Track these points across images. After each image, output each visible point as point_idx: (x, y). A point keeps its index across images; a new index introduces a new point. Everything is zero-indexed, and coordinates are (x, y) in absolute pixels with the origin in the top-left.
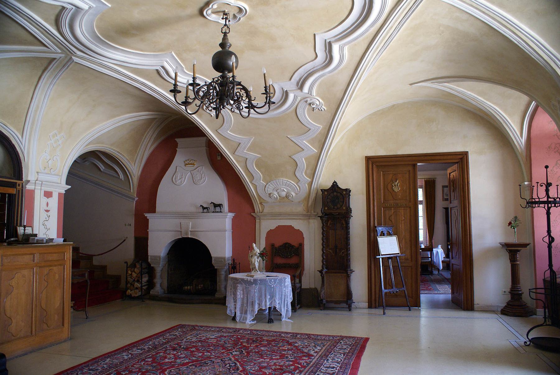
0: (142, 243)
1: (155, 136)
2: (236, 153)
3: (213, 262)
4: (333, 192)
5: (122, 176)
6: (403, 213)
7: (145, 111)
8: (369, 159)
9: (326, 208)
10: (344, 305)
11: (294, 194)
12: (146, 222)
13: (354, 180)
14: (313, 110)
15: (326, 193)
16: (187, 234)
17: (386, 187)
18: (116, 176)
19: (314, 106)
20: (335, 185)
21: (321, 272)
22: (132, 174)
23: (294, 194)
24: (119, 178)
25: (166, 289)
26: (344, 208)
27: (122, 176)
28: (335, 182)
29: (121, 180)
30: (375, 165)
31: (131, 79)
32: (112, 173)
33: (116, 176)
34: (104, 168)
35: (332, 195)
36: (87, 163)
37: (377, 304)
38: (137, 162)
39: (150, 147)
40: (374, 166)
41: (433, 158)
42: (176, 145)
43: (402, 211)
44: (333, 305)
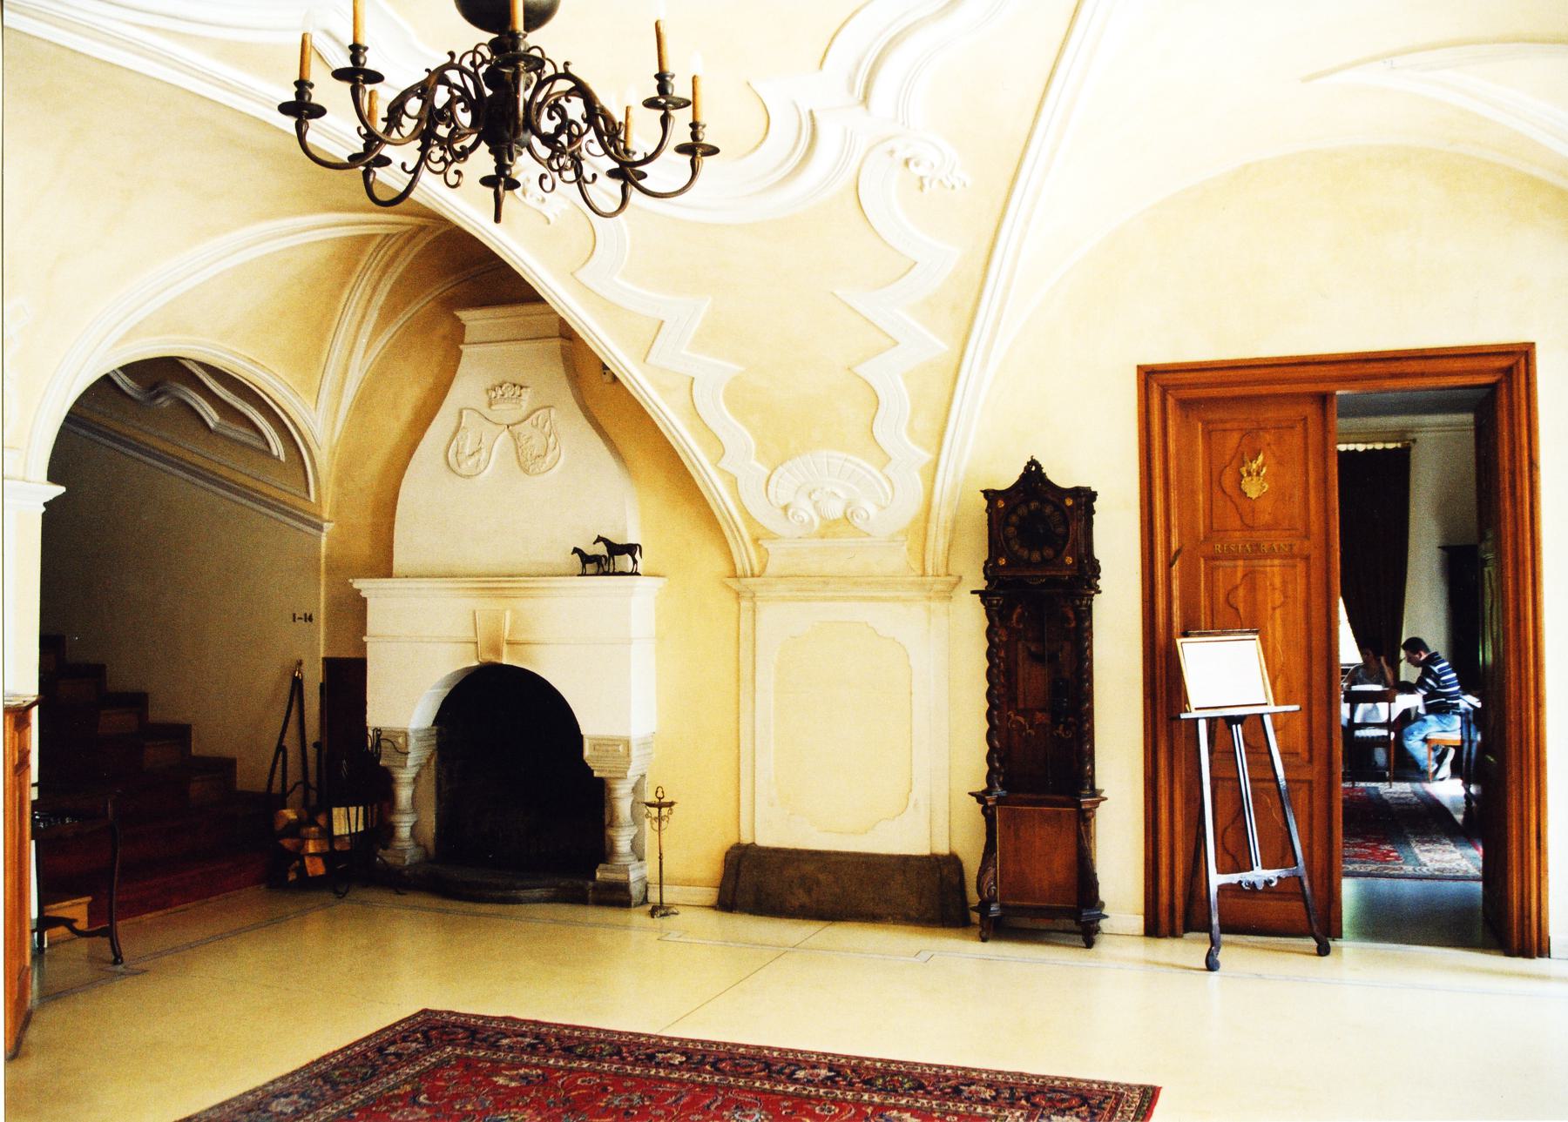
0: (347, 678)
1: (380, 299)
2: (651, 359)
3: (587, 752)
4: (1026, 502)
5: (277, 447)
6: (1277, 581)
7: (312, 211)
8: (1148, 375)
9: (1002, 562)
10: (1070, 924)
11: (873, 510)
12: (359, 607)
13: (1100, 456)
14: (922, 188)
15: (1001, 504)
16: (497, 650)
17: (1215, 480)
18: (262, 446)
19: (920, 171)
20: (1033, 475)
21: (980, 797)
22: (309, 438)
23: (873, 510)
24: (267, 452)
25: (431, 844)
26: (1069, 560)
27: (277, 447)
28: (1033, 462)
29: (278, 458)
30: (1187, 403)
31: (226, 86)
32: (242, 433)
33: (262, 446)
34: (216, 417)
35: (1022, 511)
36: (164, 402)
37: (1179, 922)
38: (323, 396)
39: (369, 346)
40: (1171, 402)
41: (1395, 367)
42: (457, 335)
43: (1273, 570)
44: (1026, 923)
